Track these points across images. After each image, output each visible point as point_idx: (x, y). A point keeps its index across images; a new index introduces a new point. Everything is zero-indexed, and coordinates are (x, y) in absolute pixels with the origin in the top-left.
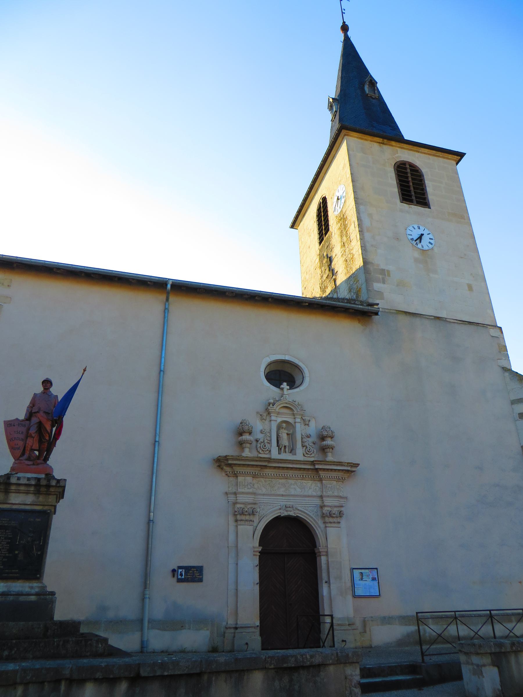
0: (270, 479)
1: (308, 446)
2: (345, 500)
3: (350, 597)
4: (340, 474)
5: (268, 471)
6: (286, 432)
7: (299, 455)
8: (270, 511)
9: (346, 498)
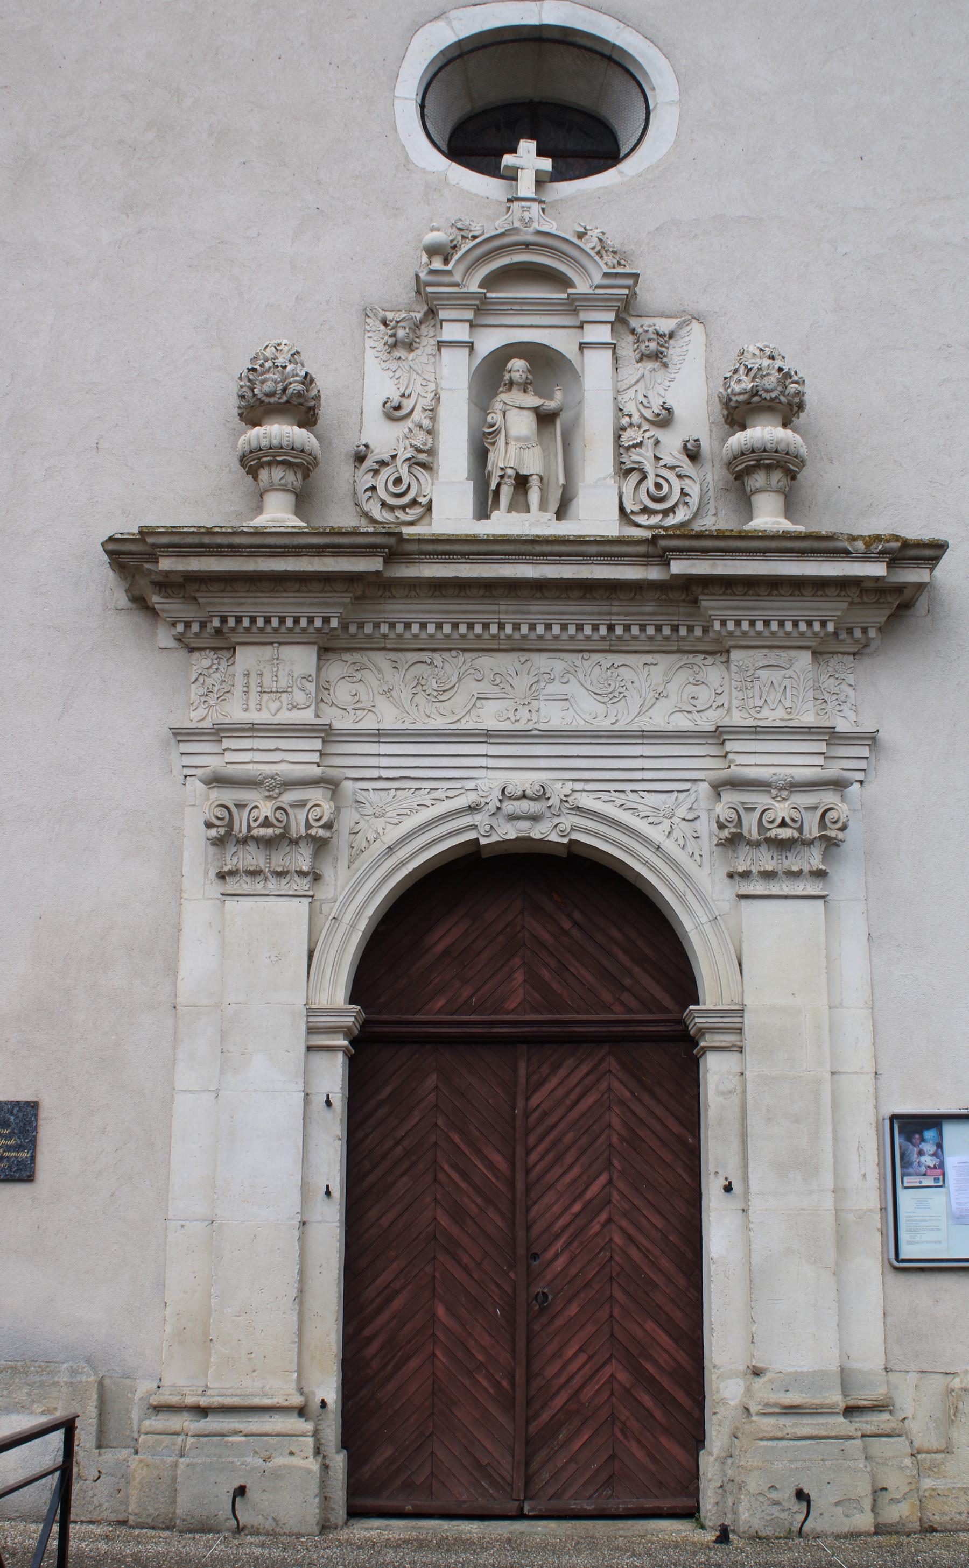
0: (424, 656)
1: (649, 468)
2: (865, 752)
3: (869, 1262)
4: (832, 609)
5: (398, 610)
6: (532, 400)
7: (596, 516)
8: (400, 826)
9: (871, 739)
